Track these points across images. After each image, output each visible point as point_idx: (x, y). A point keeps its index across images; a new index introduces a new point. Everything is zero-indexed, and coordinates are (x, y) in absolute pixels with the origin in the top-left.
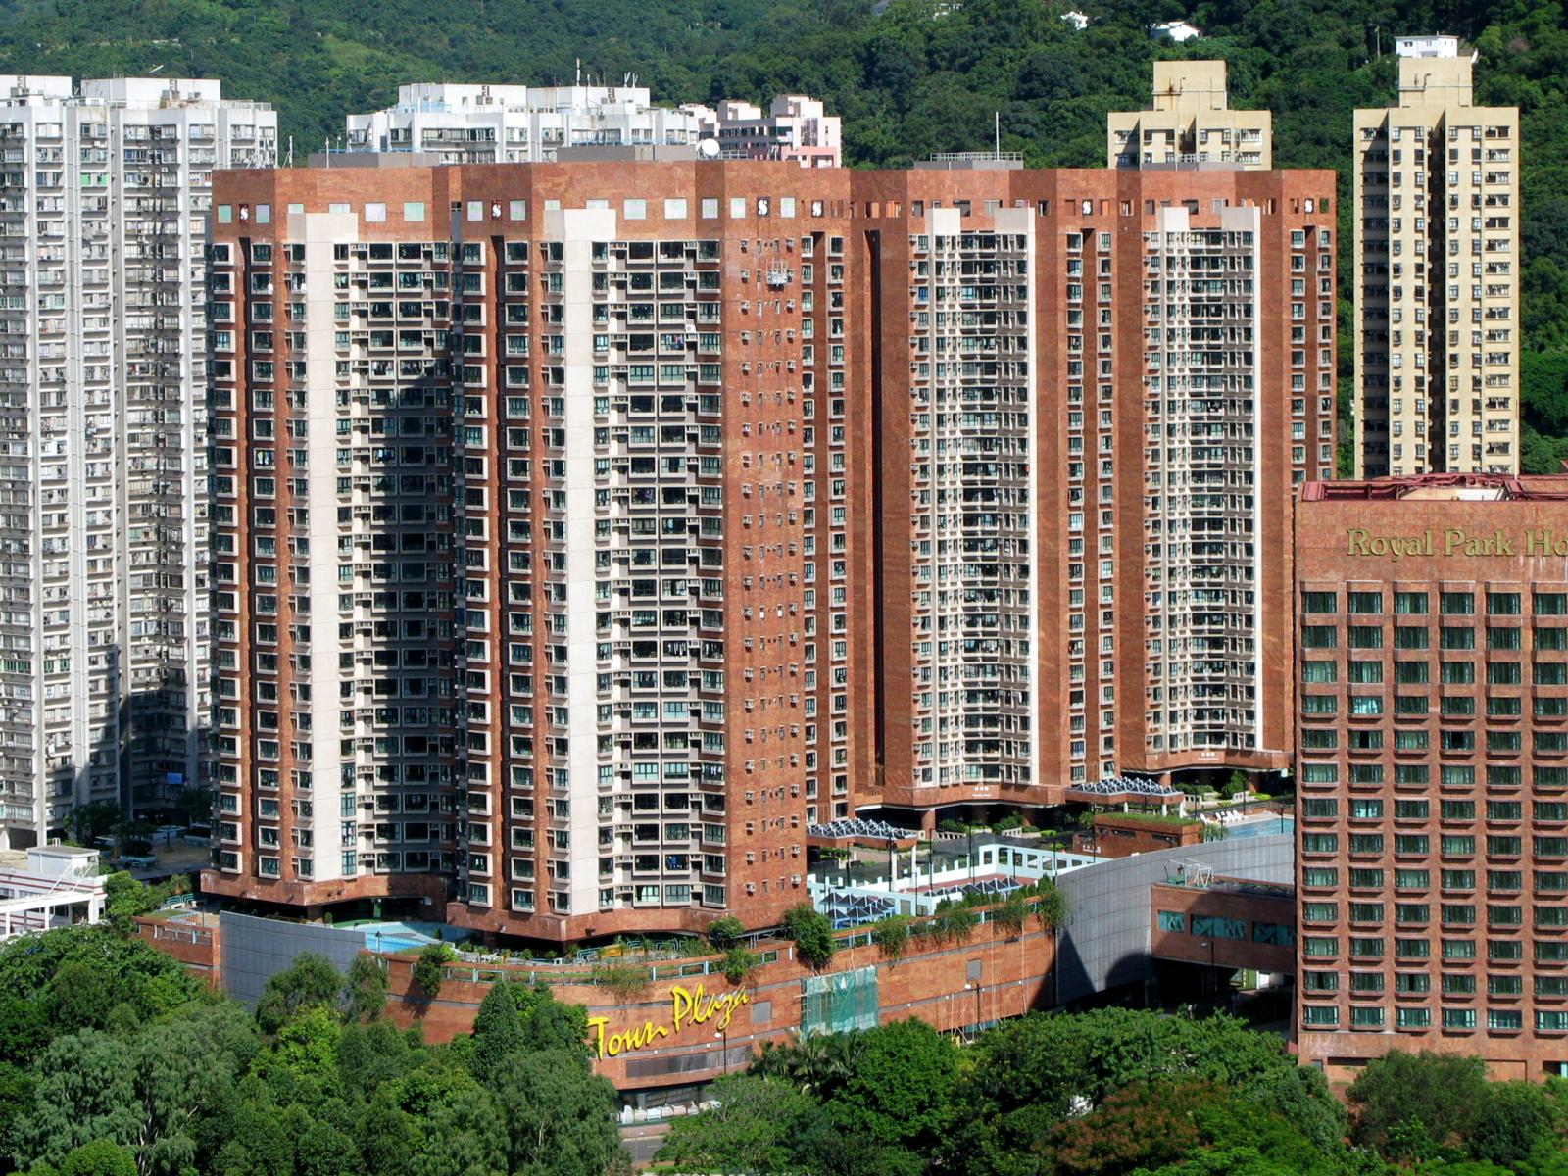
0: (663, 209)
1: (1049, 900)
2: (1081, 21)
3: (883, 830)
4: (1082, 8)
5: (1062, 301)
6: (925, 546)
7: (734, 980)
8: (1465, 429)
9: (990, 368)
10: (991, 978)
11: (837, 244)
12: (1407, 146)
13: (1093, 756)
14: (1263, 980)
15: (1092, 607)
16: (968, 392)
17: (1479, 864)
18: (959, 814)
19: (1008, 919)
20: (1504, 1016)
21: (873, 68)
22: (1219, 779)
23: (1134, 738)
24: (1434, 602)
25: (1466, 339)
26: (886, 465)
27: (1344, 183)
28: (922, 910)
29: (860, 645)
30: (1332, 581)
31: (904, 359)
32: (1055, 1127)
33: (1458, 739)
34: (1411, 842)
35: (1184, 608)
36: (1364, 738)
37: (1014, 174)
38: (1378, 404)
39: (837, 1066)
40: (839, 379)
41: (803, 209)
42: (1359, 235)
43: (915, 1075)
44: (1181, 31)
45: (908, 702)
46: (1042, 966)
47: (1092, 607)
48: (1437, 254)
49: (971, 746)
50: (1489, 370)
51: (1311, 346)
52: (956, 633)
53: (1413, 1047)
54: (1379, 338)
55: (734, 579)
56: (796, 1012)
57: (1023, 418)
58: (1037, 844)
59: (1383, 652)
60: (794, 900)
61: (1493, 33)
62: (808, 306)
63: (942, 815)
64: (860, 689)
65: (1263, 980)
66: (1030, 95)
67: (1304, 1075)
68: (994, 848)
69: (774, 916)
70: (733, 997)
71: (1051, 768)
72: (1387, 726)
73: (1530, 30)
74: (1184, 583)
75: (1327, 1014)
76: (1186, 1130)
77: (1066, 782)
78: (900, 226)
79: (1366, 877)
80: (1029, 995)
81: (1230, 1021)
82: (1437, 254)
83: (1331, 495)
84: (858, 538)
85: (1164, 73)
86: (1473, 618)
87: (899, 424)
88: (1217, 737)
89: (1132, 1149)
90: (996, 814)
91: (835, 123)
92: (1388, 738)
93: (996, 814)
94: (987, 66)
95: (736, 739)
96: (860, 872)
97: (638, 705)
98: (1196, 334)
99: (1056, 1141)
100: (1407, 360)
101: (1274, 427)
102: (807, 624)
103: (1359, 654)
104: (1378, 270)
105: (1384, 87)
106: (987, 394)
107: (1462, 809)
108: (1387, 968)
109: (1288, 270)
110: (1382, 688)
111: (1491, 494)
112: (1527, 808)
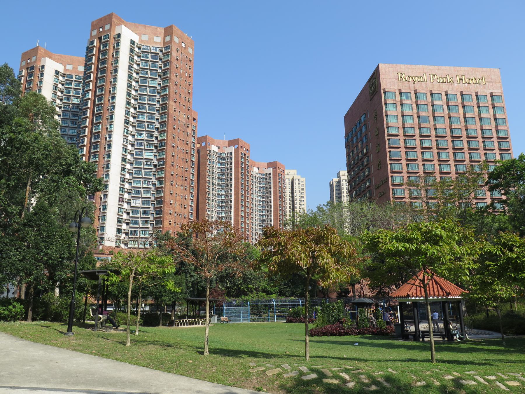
0: (154, 39)
5: (240, 166)
87: (204, 189)
97: (135, 181)
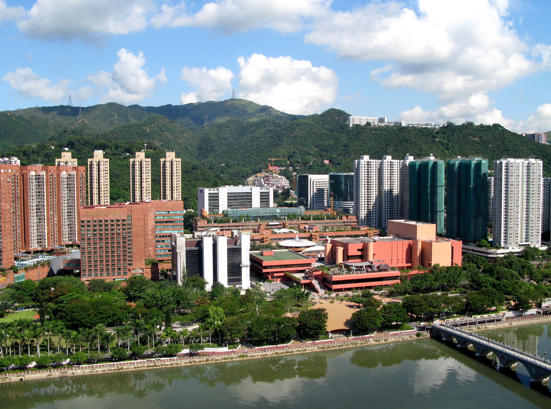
1: (49, 263)
2: (53, 148)
3: (25, 254)
4: (54, 146)
6: (31, 216)
7: (4, 276)
8: (103, 200)
9: (39, 192)
10: (41, 273)
11: (17, 176)
12: (137, 163)
13: (54, 243)
14: (78, 271)
15: (54, 224)
16: (36, 196)
17: (104, 255)
18: (36, 252)
19: (43, 265)
20: (108, 273)
21: (25, 153)
22: (72, 246)
23: (60, 240)
24: (98, 221)
25: (103, 188)
26: (25, 206)
27: (87, 169)
28: (31, 265)
29: (22, 230)
30: (84, 219)
31: (27, 191)
32: (49, 292)
33: (101, 239)
34: (96, 252)
35: (66, 224)
36: (89, 239)
37: (42, 167)
38: (92, 197)
39: (19, 286)
40: (18, 194)
41: (12, 171)
42: (89, 175)
43: (30, 287)
44: (66, 149)
45: (29, 237)
46: (48, 271)
47: (54, 224)
48: (99, 177)
49: (38, 243)
50: (106, 192)
51: (83, 189)
52: (35, 228)
53: (96, 278)
54: (92, 188)
55: (3, 221)
56: (13, 279)
57: (44, 199)
58: (47, 255)
59: (91, 228)
60: (12, 264)
61: (107, 150)
62: (13, 184)
63: (34, 252)
64: (22, 236)
65: (78, 271)
66: (46, 157)
67: (82, 283)
68: (41, 256)
69: (10, 267)
70: (4, 278)
71: (49, 245)
72: (92, 238)
73: (111, 150)
74: (66, 220)
75: (85, 275)
76: (66, 291)
77: (51, 247)
78: (27, 174)
79: (90, 257)
80: (46, 275)
81: (72, 276)
82: (99, 177)
83: (84, 208)
84: (21, 216)
85: (63, 154)
86: (103, 223)
88: (71, 240)
89: (59, 294)
90: (41, 252)
91: (19, 161)
92: (92, 239)
93: (41, 252)
94: (40, 153)
95: (4, 243)
96: (23, 260)
98: (67, 188)
99: (49, 294)
100: (95, 191)
101: (78, 200)
102: (14, 227)
103: (88, 228)
104: (91, 179)
105: (92, 157)
106: (39, 196)
107: (102, 247)
108: (93, 269)
109: (79, 179)
110: (91, 232)
111: (105, 207)
112: (110, 247)
